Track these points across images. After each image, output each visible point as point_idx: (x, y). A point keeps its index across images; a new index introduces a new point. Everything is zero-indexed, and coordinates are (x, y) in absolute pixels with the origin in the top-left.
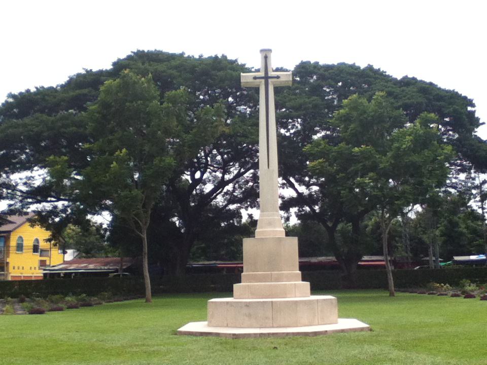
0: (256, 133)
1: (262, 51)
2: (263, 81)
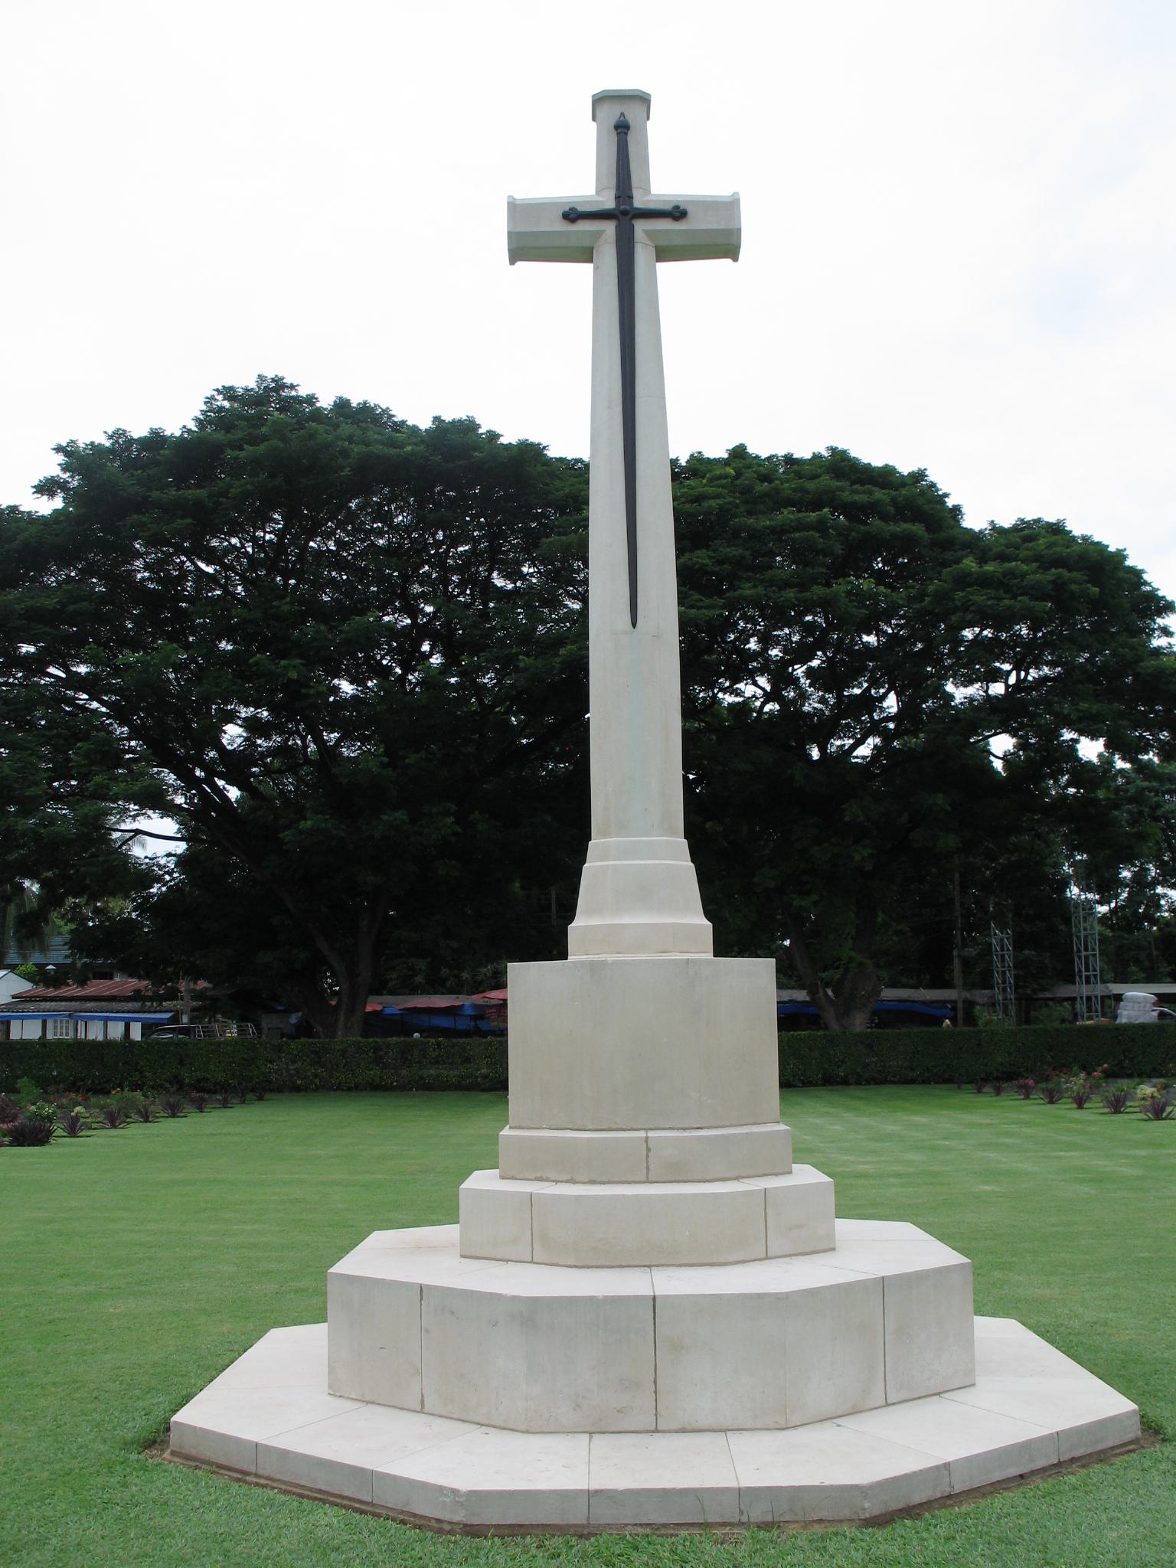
0: (214, 1373)
1: (601, 100)
2: (609, 228)
